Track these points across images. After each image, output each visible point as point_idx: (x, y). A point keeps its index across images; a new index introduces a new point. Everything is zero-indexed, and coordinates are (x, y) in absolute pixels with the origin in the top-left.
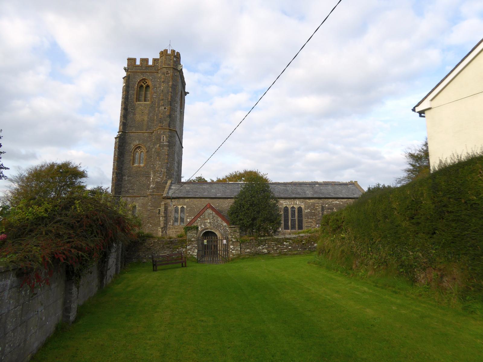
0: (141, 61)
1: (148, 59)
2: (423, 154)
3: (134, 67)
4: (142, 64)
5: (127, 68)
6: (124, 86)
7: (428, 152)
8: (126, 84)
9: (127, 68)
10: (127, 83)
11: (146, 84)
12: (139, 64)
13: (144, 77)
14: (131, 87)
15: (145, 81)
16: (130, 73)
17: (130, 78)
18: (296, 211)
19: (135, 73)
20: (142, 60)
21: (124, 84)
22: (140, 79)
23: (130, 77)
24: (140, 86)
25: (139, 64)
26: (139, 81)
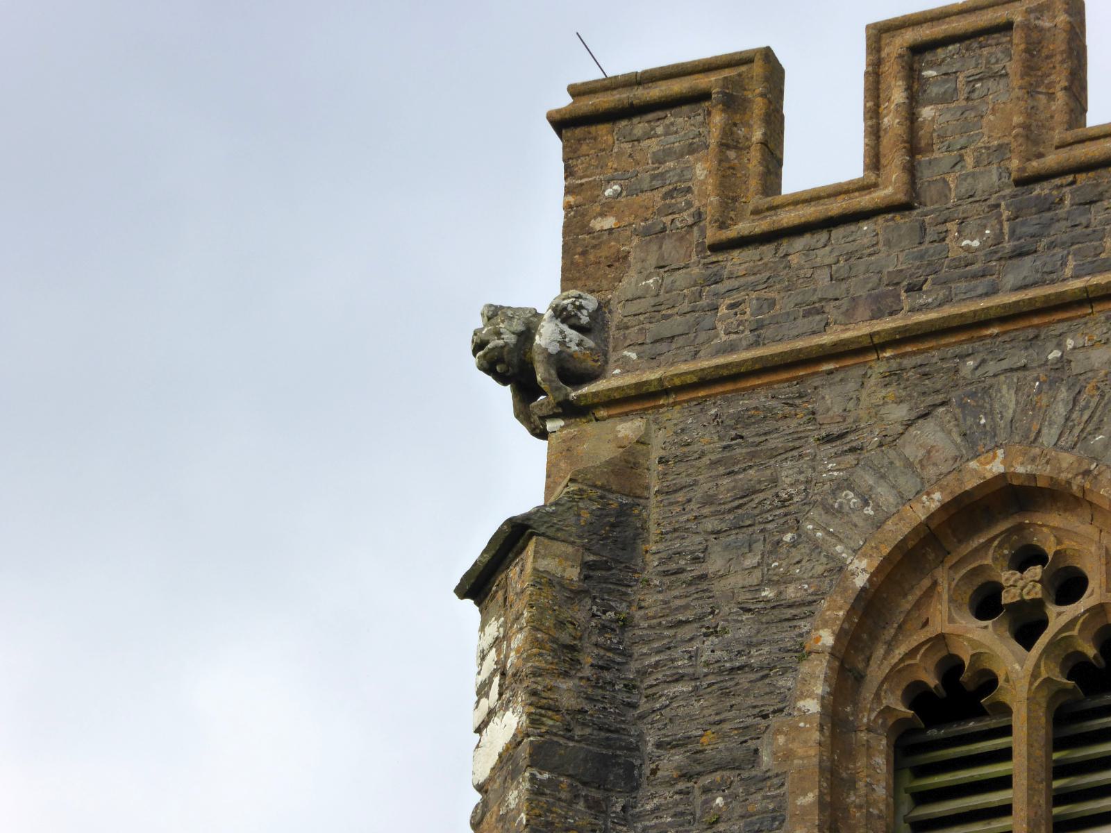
0: (898, 95)
1: (879, 34)
2: (972, 314)
3: (737, 260)
4: (913, 146)
5: (561, 313)
6: (507, 761)
7: (563, 238)
8: (540, 707)
9: (547, 336)
10: (567, 692)
11: (1059, 616)
12: (852, 167)
13: (973, 443)
14: (671, 762)
15: (1027, 557)
16: (628, 429)
17: (653, 552)
18: (624, 589)
19: (758, 398)
20: (918, 50)
21: (508, 724)
22: (897, 530)
23: (654, 512)
24: (918, 697)
25: (852, 167)
26: (861, 571)
